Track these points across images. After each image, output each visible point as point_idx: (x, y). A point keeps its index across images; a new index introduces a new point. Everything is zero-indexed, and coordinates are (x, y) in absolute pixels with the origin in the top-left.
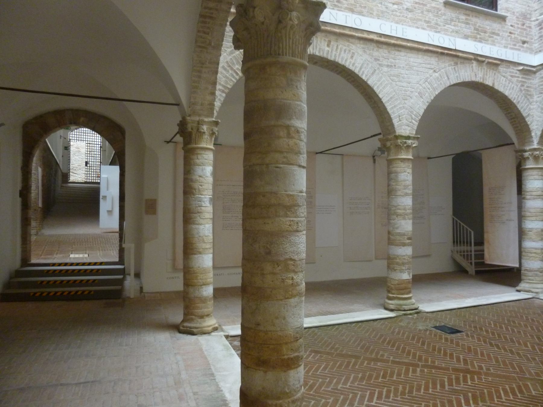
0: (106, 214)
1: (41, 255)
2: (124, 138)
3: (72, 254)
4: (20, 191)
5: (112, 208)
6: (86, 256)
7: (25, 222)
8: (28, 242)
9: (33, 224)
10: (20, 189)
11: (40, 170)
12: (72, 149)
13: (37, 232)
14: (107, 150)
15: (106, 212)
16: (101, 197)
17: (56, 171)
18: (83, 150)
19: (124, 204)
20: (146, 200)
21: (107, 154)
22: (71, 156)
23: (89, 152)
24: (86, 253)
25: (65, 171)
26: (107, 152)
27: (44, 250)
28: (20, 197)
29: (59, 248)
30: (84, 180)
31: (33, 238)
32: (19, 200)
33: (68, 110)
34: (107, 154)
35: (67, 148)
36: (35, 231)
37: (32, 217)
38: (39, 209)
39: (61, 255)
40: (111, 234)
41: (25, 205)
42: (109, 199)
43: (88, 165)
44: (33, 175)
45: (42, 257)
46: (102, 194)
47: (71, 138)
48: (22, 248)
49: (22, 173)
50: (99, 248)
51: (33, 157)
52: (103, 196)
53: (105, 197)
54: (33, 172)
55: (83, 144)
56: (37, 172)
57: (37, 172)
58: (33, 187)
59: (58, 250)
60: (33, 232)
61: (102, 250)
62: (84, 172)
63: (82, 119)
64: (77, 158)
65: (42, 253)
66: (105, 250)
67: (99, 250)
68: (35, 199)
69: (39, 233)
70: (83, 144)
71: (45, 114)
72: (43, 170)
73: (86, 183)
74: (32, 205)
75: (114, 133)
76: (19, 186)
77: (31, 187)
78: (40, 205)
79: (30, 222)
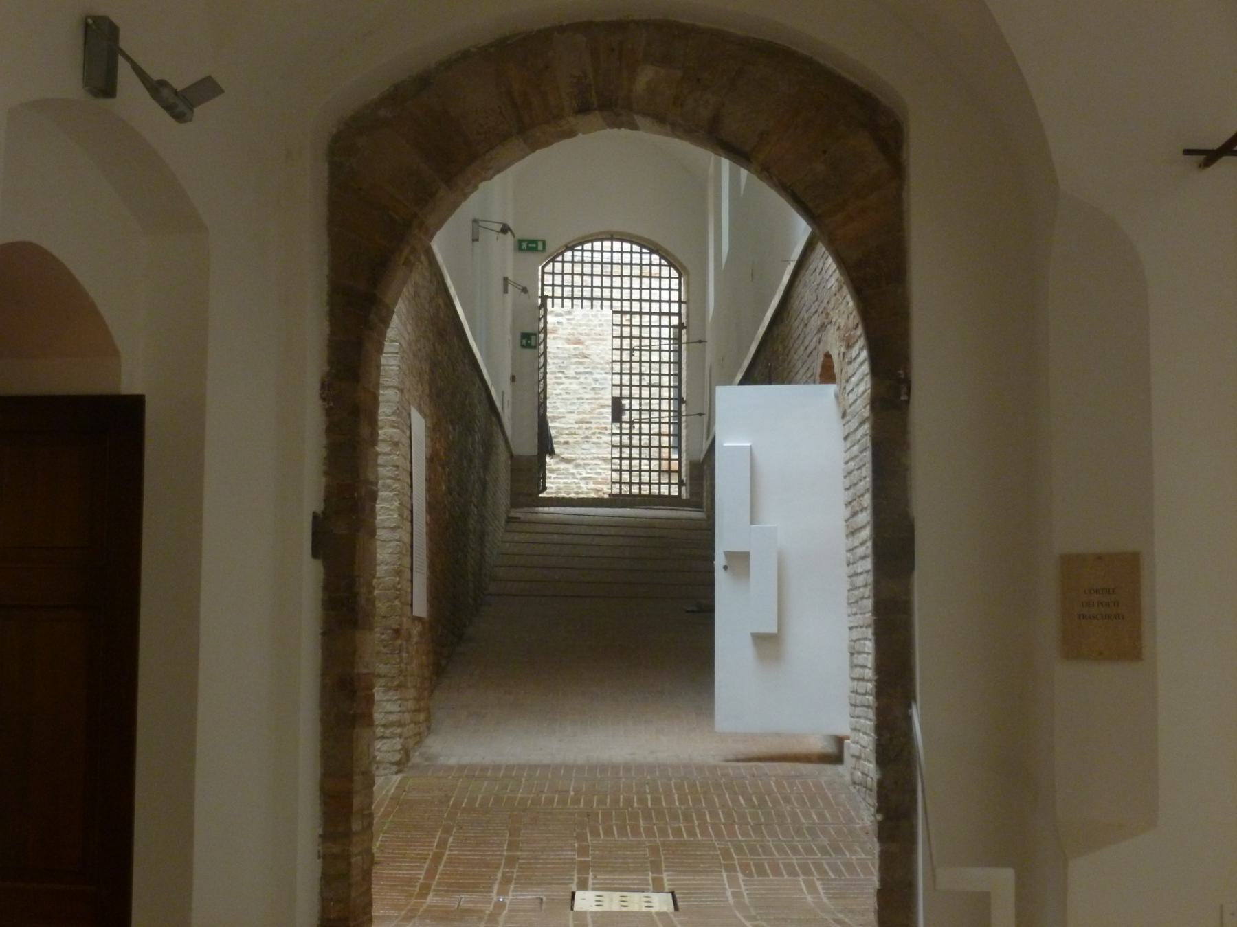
0: (748, 650)
1: (423, 894)
2: (898, 170)
3: (583, 886)
4: (315, 517)
5: (779, 630)
6: (660, 903)
7: (344, 703)
8: (356, 826)
9: (387, 706)
10: (319, 507)
11: (419, 424)
12: (555, 346)
13: (406, 752)
14: (708, 337)
15: (749, 640)
16: (719, 561)
17: (488, 442)
18: (602, 350)
19: (908, 591)
20: (1071, 564)
21: (709, 358)
22: (550, 379)
23: (629, 352)
24: (658, 888)
25: (526, 446)
26: (710, 347)
27: (437, 858)
28: (315, 555)
29: (513, 846)
30: (606, 490)
31: (386, 784)
32: (309, 574)
33: (562, 29)
34: (709, 358)
35: (532, 340)
36: (397, 743)
37: (382, 668)
38: (416, 630)
39: (530, 895)
40: (787, 766)
41: (344, 606)
42: (762, 571)
43: (626, 417)
44: (381, 448)
45: (430, 899)
46: (725, 542)
47: (548, 292)
48: (326, 857)
49: (328, 412)
50: (726, 854)
51: (386, 322)
52: (729, 555)
53: (740, 561)
54: (385, 432)
55: (604, 314)
56: (404, 438)
57: (404, 438)
58: (386, 511)
59: (511, 862)
60: (385, 749)
61: (745, 869)
62: (606, 452)
63: (646, 76)
64: (574, 386)
65: (431, 874)
66: (761, 872)
67: (730, 869)
68: (398, 573)
69: (416, 759)
70: (604, 314)
71: (448, 64)
72: (434, 430)
73: (616, 500)
74: (381, 607)
75: (830, 144)
76: (311, 496)
77: (373, 497)
78: (421, 608)
79: (370, 700)
